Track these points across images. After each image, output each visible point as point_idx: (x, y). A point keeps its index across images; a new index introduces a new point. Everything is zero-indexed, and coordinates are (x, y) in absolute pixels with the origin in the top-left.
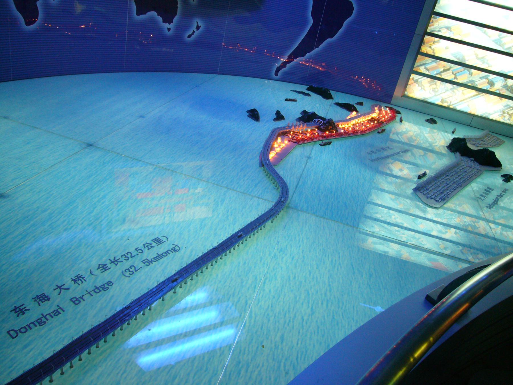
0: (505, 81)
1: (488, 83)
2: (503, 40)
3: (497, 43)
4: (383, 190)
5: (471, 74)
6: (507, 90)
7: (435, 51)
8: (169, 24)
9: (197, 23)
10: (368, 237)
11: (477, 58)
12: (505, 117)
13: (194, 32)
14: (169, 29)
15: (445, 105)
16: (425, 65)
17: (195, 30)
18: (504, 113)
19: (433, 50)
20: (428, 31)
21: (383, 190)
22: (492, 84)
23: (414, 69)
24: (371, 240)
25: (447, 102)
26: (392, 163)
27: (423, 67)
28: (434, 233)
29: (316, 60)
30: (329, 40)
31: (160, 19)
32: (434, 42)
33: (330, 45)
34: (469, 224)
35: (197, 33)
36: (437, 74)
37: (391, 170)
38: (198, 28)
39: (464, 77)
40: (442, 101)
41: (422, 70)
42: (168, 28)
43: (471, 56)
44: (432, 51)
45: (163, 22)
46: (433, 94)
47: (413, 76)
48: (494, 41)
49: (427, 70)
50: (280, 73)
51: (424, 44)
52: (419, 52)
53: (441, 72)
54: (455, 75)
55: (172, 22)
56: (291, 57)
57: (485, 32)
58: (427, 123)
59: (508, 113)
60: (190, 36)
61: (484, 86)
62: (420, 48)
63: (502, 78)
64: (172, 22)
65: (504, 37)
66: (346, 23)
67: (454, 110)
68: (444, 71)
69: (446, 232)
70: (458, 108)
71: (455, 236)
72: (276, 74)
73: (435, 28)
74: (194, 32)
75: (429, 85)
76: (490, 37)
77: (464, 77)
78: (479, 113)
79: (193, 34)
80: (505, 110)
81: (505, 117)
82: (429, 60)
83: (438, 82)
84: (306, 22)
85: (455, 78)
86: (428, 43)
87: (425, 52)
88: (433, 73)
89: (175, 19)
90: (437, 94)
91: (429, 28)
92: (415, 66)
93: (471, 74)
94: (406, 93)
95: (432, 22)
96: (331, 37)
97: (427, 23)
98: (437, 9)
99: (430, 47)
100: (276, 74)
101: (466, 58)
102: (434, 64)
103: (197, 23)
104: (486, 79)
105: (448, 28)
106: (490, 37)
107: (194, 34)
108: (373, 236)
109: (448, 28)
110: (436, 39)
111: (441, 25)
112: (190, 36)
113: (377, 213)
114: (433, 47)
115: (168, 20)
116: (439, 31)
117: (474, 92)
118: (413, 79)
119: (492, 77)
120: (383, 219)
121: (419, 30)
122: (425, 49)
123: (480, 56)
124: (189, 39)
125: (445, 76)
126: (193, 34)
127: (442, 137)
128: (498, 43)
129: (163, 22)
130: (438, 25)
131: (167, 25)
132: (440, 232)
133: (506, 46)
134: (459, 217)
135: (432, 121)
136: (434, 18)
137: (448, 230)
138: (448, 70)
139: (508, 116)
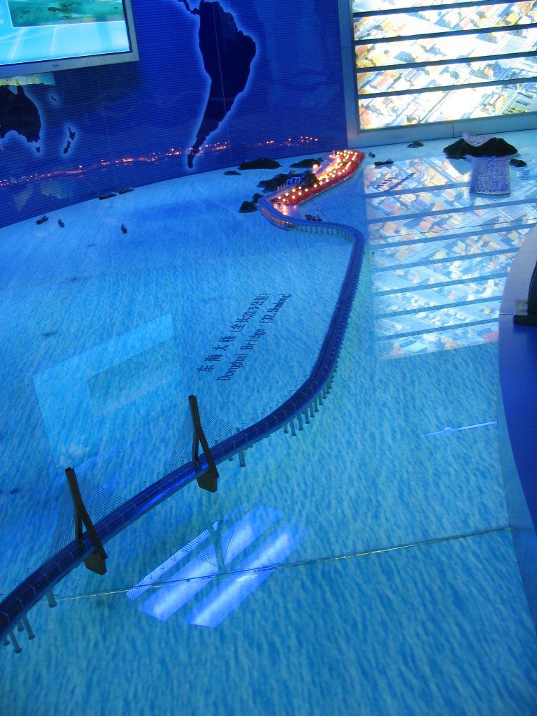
0: (469, 65)
1: (451, 76)
2: (447, 18)
3: (440, 25)
4: (384, 270)
5: (427, 73)
6: (476, 76)
7: (374, 61)
8: (36, 142)
9: (69, 128)
10: (393, 341)
11: (427, 51)
12: (488, 110)
13: (69, 143)
14: (38, 149)
15: (415, 122)
16: (370, 84)
17: (70, 140)
18: (485, 105)
19: (371, 60)
20: (356, 40)
21: (384, 270)
22: (456, 76)
23: (359, 93)
24: (397, 343)
25: (415, 119)
26: (382, 228)
27: (368, 86)
28: (471, 298)
29: (220, 139)
30: (239, 96)
31: (23, 138)
32: (368, 51)
33: (244, 102)
34: (507, 264)
35: (73, 143)
36: (389, 88)
37: (385, 238)
38: (72, 135)
39: (421, 80)
40: (409, 119)
41: (368, 90)
42: (36, 147)
43: (417, 51)
44: (370, 62)
45: (28, 141)
46: (394, 115)
47: (361, 102)
48: (436, 23)
49: (375, 87)
50: (194, 161)
51: (357, 57)
52: (356, 70)
53: (392, 84)
54: (409, 81)
55: (39, 138)
56: (199, 143)
57: (421, 17)
58: (411, 148)
59: (489, 104)
60: (66, 151)
61: (450, 81)
62: (355, 64)
63: (464, 64)
64: (39, 138)
65: (446, 14)
66: (252, 65)
67: (428, 125)
68: (395, 81)
69: (485, 289)
70: (431, 120)
71: (496, 288)
72: (190, 165)
73: (362, 33)
74: (69, 143)
75: (385, 105)
76: (429, 20)
77: (421, 80)
78: (457, 117)
79: (68, 146)
80: (484, 101)
81: (488, 110)
82: (371, 75)
83: (394, 98)
84: (203, 81)
85: (412, 85)
86: (361, 54)
87: (363, 67)
88: (383, 89)
89: (42, 133)
90: (399, 113)
91: (356, 35)
92: (359, 87)
93: (427, 73)
94: (361, 127)
95: (356, 27)
96: (241, 90)
97: (352, 31)
98: (356, 9)
99: (366, 58)
100: (190, 165)
101: (414, 56)
102: (380, 78)
103: (69, 128)
104: (448, 71)
105: (378, 27)
106: (429, 20)
107: (71, 145)
108: (398, 336)
109: (378, 27)
110: (369, 46)
111: (368, 27)
112: (66, 151)
113: (389, 305)
114: (370, 56)
115: (33, 136)
116: (368, 35)
117: (440, 94)
118: (362, 105)
119: (452, 67)
120: (401, 310)
121: (344, 42)
122: (361, 63)
123: (428, 48)
124: (67, 154)
125: (398, 87)
126: (68, 146)
127: (427, 165)
128: (442, 24)
129: (28, 141)
130: (364, 27)
131: (34, 145)
132: (478, 292)
133: (452, 25)
134: (491, 260)
135: (417, 144)
136: (356, 21)
137: (486, 286)
138: (399, 78)
139: (491, 107)
